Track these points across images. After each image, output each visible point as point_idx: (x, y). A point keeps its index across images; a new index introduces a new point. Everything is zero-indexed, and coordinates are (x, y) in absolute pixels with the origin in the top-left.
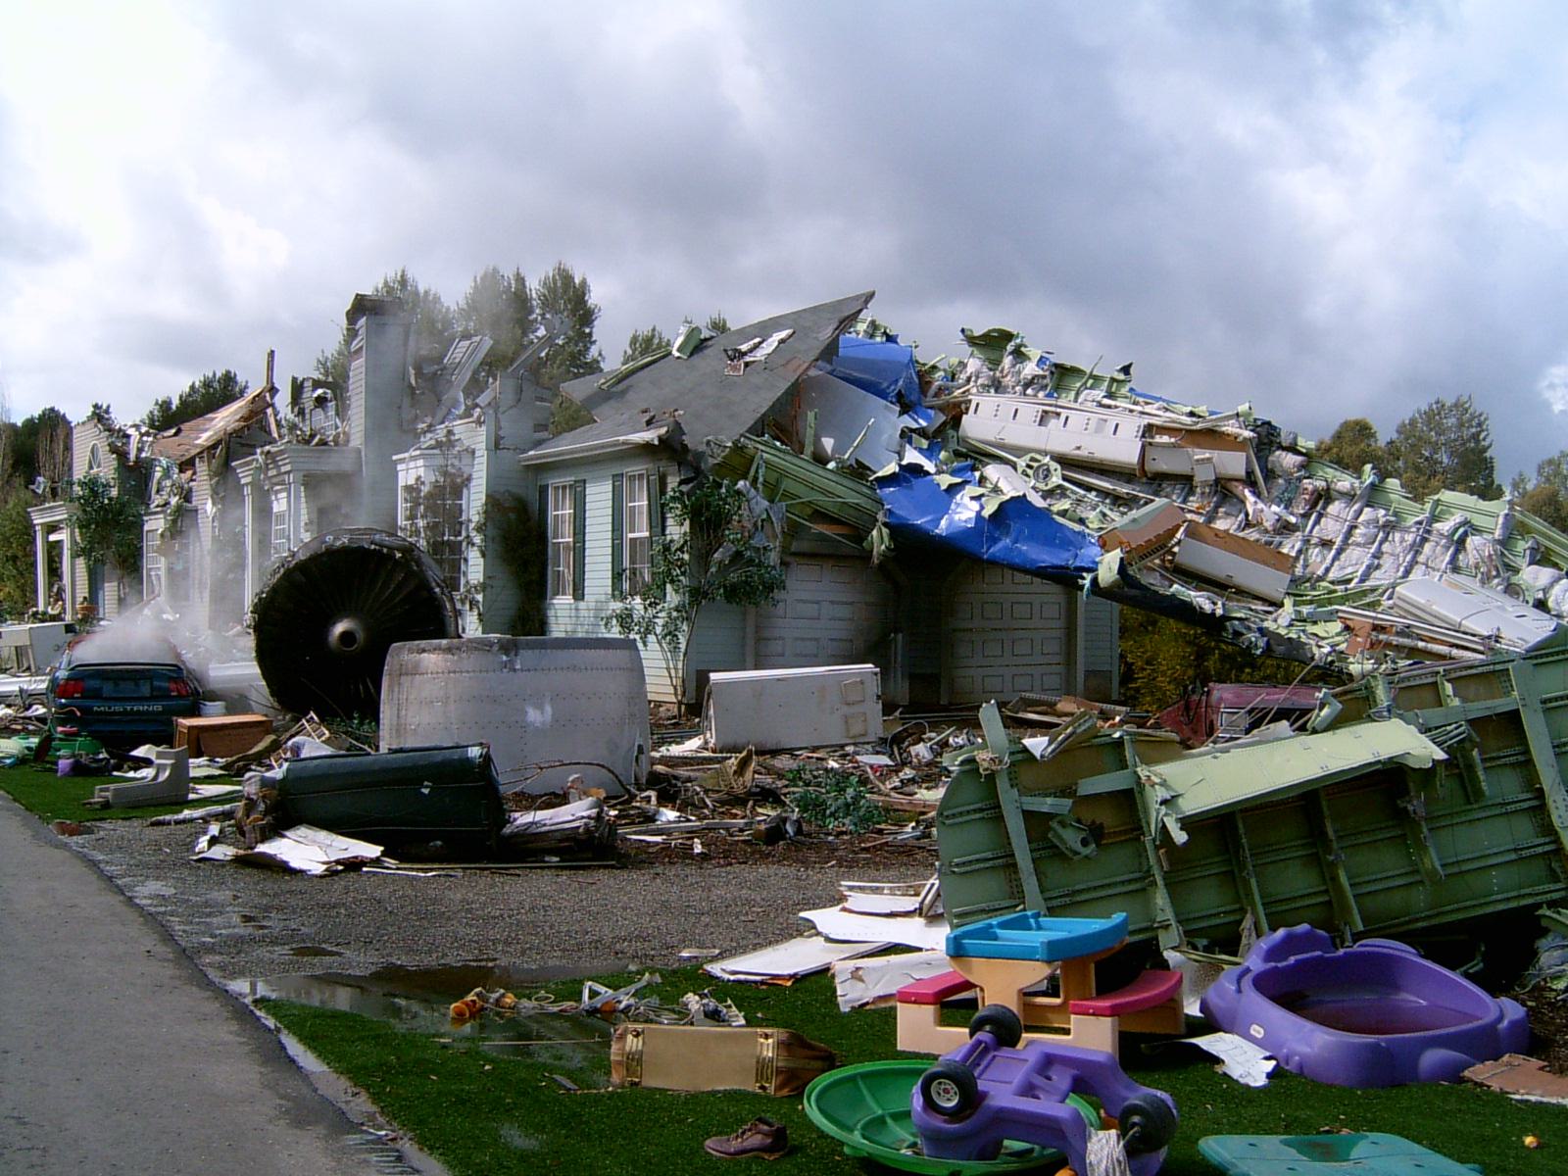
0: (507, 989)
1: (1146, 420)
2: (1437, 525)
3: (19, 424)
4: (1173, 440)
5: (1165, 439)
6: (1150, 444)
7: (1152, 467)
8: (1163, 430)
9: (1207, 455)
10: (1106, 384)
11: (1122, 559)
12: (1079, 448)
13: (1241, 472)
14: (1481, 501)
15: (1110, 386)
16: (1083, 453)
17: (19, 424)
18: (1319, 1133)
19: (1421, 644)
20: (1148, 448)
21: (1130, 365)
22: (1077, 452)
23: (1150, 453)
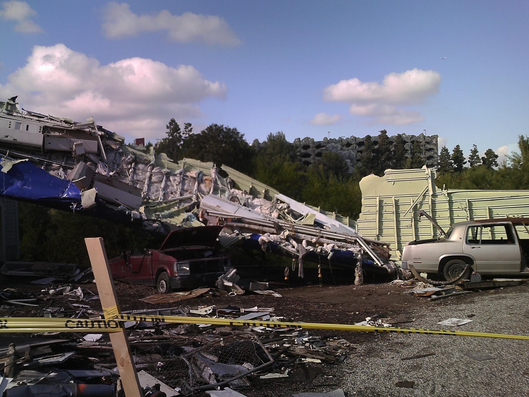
0: (424, 282)
1: (44, 124)
2: (188, 174)
3: (267, 141)
4: (61, 134)
5: (57, 134)
6: (48, 136)
7: (48, 147)
8: (54, 129)
9: (80, 142)
10: (5, 106)
11: (97, 194)
12: (7, 137)
13: (95, 150)
14: (202, 163)
15: (7, 107)
16: (10, 139)
17: (267, 141)
18: (504, 334)
19: (247, 226)
20: (46, 138)
21: (458, 146)
22: (6, 139)
23: (48, 140)
